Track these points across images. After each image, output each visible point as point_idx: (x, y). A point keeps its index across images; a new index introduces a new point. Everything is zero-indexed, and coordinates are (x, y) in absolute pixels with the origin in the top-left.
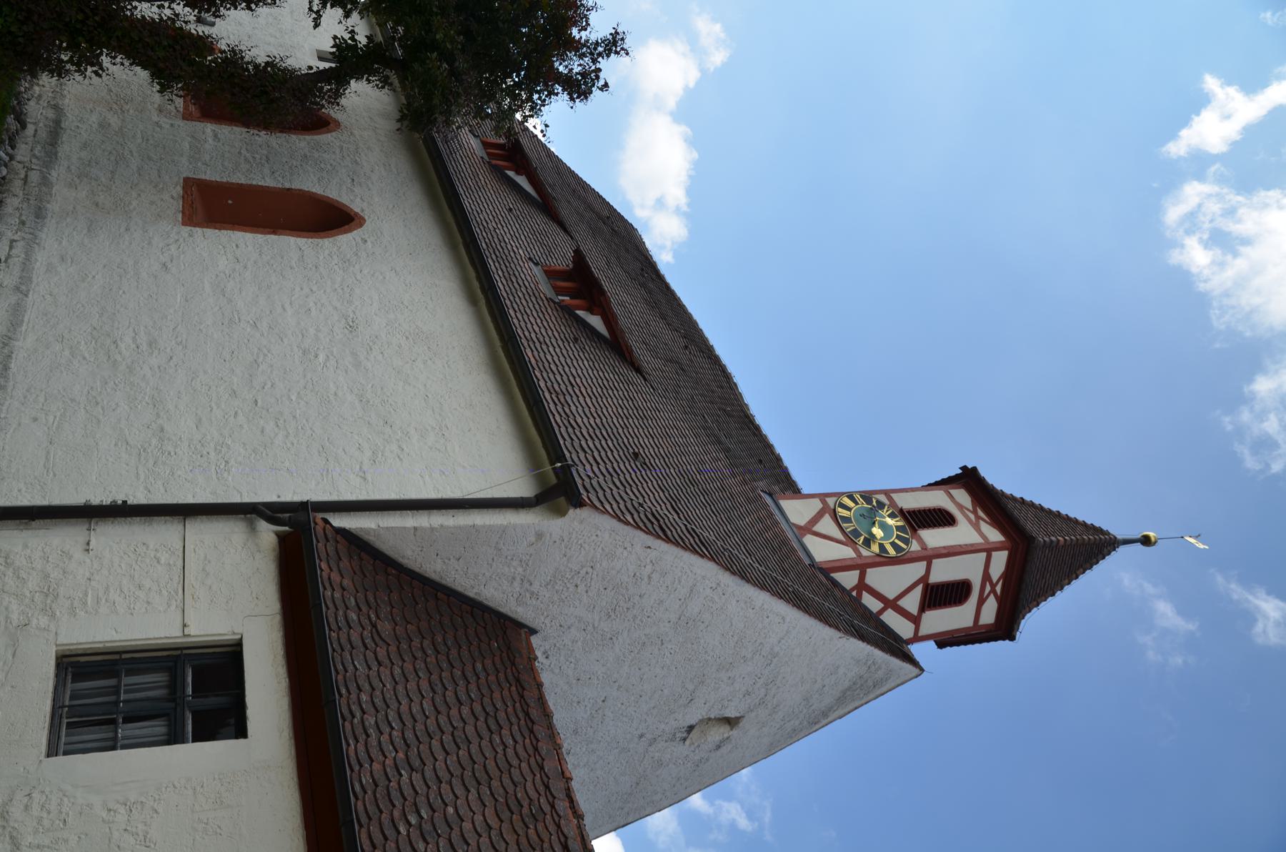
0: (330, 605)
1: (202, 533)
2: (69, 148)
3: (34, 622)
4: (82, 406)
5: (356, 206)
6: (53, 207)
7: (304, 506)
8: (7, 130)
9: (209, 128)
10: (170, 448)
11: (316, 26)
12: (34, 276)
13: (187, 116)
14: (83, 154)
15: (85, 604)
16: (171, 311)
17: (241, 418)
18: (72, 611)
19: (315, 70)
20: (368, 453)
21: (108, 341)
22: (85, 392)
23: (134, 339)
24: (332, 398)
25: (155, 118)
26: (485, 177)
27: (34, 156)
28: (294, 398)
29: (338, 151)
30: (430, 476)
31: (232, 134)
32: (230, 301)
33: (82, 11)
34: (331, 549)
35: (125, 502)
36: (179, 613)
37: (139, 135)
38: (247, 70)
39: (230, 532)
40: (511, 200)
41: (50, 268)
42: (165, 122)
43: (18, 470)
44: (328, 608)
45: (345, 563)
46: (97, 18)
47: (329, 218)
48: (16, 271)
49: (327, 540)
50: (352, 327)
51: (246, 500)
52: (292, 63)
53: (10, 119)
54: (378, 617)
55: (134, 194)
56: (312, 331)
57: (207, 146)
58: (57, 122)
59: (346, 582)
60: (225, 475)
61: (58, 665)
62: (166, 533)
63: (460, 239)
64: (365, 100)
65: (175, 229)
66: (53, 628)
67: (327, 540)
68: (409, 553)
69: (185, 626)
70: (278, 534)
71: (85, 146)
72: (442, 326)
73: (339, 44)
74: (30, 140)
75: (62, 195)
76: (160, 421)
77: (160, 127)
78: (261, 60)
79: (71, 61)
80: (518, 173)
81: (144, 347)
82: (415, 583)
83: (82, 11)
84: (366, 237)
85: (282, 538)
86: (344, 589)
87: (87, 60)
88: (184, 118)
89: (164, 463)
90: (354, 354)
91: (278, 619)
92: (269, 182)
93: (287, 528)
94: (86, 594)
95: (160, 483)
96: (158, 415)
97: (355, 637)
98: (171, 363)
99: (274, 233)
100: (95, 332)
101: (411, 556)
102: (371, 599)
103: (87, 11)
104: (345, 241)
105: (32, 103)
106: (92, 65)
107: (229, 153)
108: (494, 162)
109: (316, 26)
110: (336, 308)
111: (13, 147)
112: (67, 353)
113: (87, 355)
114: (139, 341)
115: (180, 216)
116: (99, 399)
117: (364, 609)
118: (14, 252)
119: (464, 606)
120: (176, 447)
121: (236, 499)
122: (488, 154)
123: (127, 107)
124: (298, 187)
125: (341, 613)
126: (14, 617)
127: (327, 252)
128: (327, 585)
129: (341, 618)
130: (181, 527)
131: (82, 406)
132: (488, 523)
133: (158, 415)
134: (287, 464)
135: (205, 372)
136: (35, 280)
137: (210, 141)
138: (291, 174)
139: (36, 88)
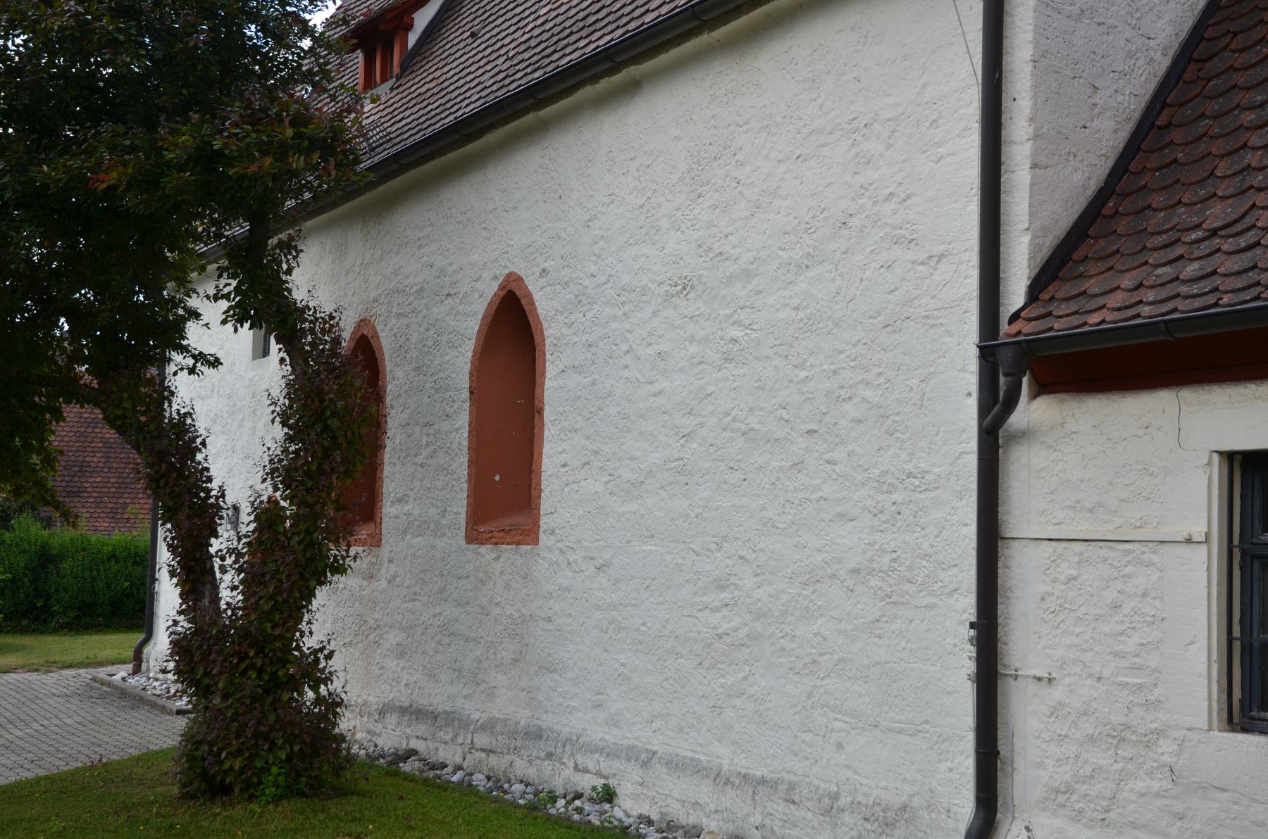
0: (1169, 306)
1: (1025, 511)
2: (436, 697)
3: (1167, 759)
4: (818, 683)
5: (490, 289)
6: (523, 716)
7: (987, 353)
8: (422, 771)
9: (389, 510)
10: (886, 559)
11: (215, 363)
12: (626, 742)
13: (375, 541)
14: (444, 678)
15: (1140, 687)
16: (669, 558)
17: (838, 454)
18: (1156, 705)
19: (282, 354)
20: (897, 251)
21: (718, 646)
22: (796, 678)
23: (715, 610)
24: (801, 314)
25: (383, 584)
26: (425, 81)
27: (452, 740)
28: (803, 374)
29: (405, 321)
30: (939, 145)
31: (396, 477)
32: (650, 474)
33: (245, 671)
34: (1065, 309)
35: (972, 625)
36: (1166, 549)
37: (410, 605)
38: (297, 452)
39: (1025, 471)
40: (456, 36)
41: (613, 722)
42: (386, 571)
43: (919, 771)
44: (1175, 310)
45: (1092, 286)
46: (252, 654)
47: (512, 328)
48: (618, 765)
49: (1049, 314)
50: (685, 287)
51: (973, 445)
52: (279, 391)
53: (406, 767)
54: (1197, 227)
55: (497, 611)
56: (693, 349)
57: (416, 512)
58: (403, 711)
59: (1127, 281)
60: (930, 477)
61: (1245, 730)
62: (1025, 570)
63: (530, 117)
64: (317, 278)
65: (543, 554)
66: (1179, 734)
67: (1049, 314)
68: (1078, 177)
69: (1189, 541)
70: (1034, 396)
71: (432, 676)
72: (678, 138)
73: (239, 315)
74: (431, 745)
75: (504, 703)
76: (842, 574)
77: (395, 577)
78: (279, 432)
79: (315, 688)
80: (409, 27)
81: (726, 596)
82: (1133, 166)
83: (245, 671)
84: (537, 271)
85: (1043, 388)
86: (1140, 285)
87: (313, 670)
88: (379, 545)
89: (910, 568)
90: (730, 281)
91: (1188, 395)
92: (463, 420)
93: (1025, 380)
94: (1126, 685)
95: (942, 575)
96: (833, 577)
97: (1234, 264)
98: (751, 557)
99: (540, 411)
100: (706, 664)
101: (1083, 175)
102: (1163, 239)
103: (243, 666)
104: (546, 305)
105: (380, 742)
106: (317, 661)
107: (425, 466)
108: (396, 69)
109: (215, 363)
110: (655, 313)
111: (444, 766)
112: (738, 702)
113: (741, 675)
114: (717, 604)
115: (524, 548)
116: (807, 660)
117: (1179, 250)
118: (591, 767)
119: (1188, 76)
120: (884, 551)
121: (972, 461)
122: (384, 80)
123: (371, 623)
124: (467, 378)
125: (1184, 289)
126: (1156, 785)
127: (565, 331)
128: (1130, 312)
129: (1195, 289)
130: (1015, 544)
131: (818, 683)
132: (1030, 36)
133: (833, 577)
134: (914, 382)
135: (763, 508)
136: (632, 742)
137: (408, 507)
138: (448, 389)
139: (359, 736)
